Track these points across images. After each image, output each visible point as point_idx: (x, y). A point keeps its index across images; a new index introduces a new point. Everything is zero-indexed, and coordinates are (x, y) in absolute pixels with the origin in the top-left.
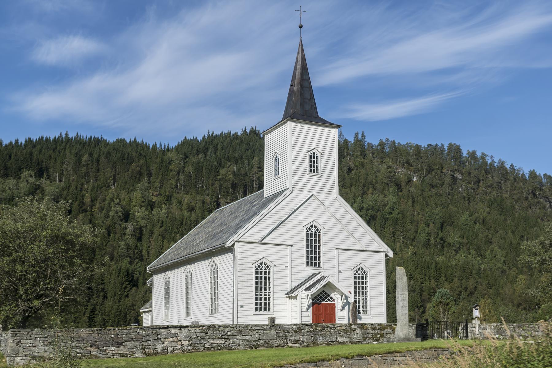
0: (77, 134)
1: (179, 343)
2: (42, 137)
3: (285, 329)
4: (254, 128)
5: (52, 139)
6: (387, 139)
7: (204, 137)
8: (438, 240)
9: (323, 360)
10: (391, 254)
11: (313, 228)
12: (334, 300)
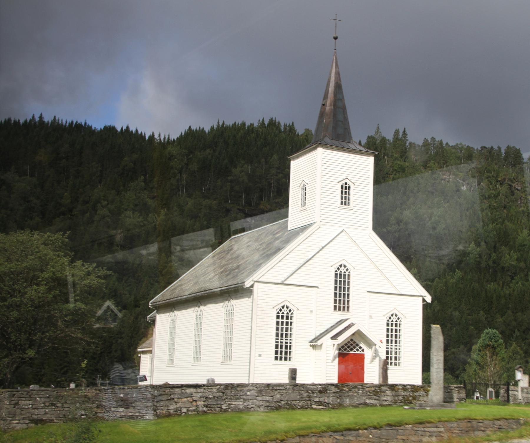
0: (55, 117)
1: (194, 403)
2: (10, 120)
3: (309, 389)
4: (274, 119)
5: (21, 122)
6: (433, 139)
7: (212, 128)
8: (491, 263)
9: (350, 430)
10: (429, 299)
11: (343, 267)
12: (363, 350)
